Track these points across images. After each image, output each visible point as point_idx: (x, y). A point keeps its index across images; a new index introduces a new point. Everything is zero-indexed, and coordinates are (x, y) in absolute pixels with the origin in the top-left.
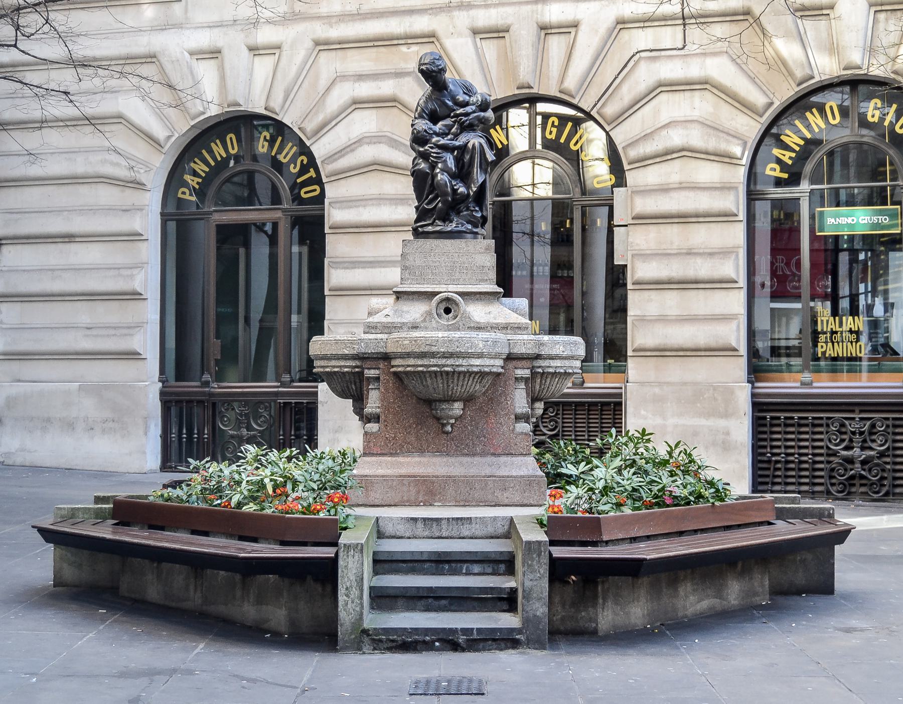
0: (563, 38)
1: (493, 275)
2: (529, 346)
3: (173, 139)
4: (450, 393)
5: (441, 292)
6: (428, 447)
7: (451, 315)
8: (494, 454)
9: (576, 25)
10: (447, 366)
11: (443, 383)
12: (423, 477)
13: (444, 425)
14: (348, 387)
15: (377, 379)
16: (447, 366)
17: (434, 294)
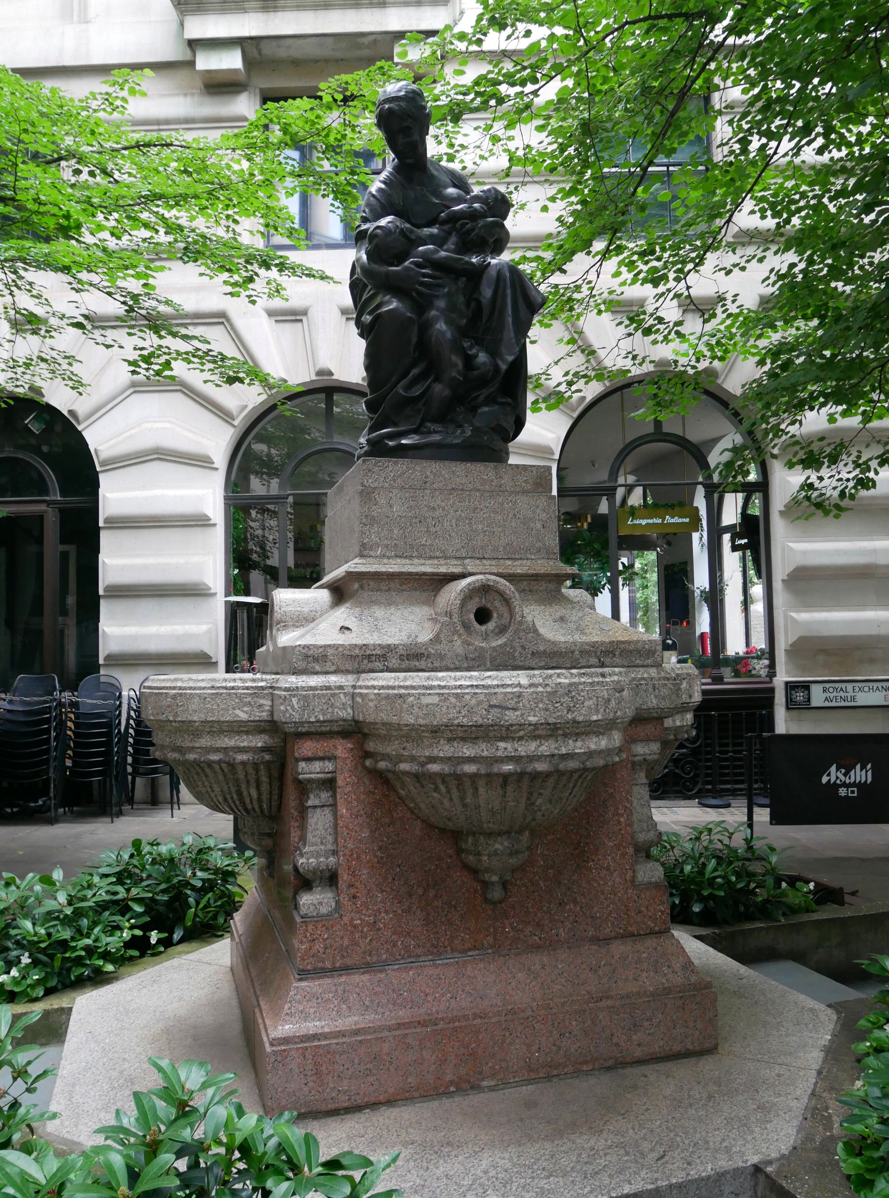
2: (664, 691)
7: (491, 625)
8: (595, 940)
12: (452, 1020)
14: (240, 794)
15: (330, 784)
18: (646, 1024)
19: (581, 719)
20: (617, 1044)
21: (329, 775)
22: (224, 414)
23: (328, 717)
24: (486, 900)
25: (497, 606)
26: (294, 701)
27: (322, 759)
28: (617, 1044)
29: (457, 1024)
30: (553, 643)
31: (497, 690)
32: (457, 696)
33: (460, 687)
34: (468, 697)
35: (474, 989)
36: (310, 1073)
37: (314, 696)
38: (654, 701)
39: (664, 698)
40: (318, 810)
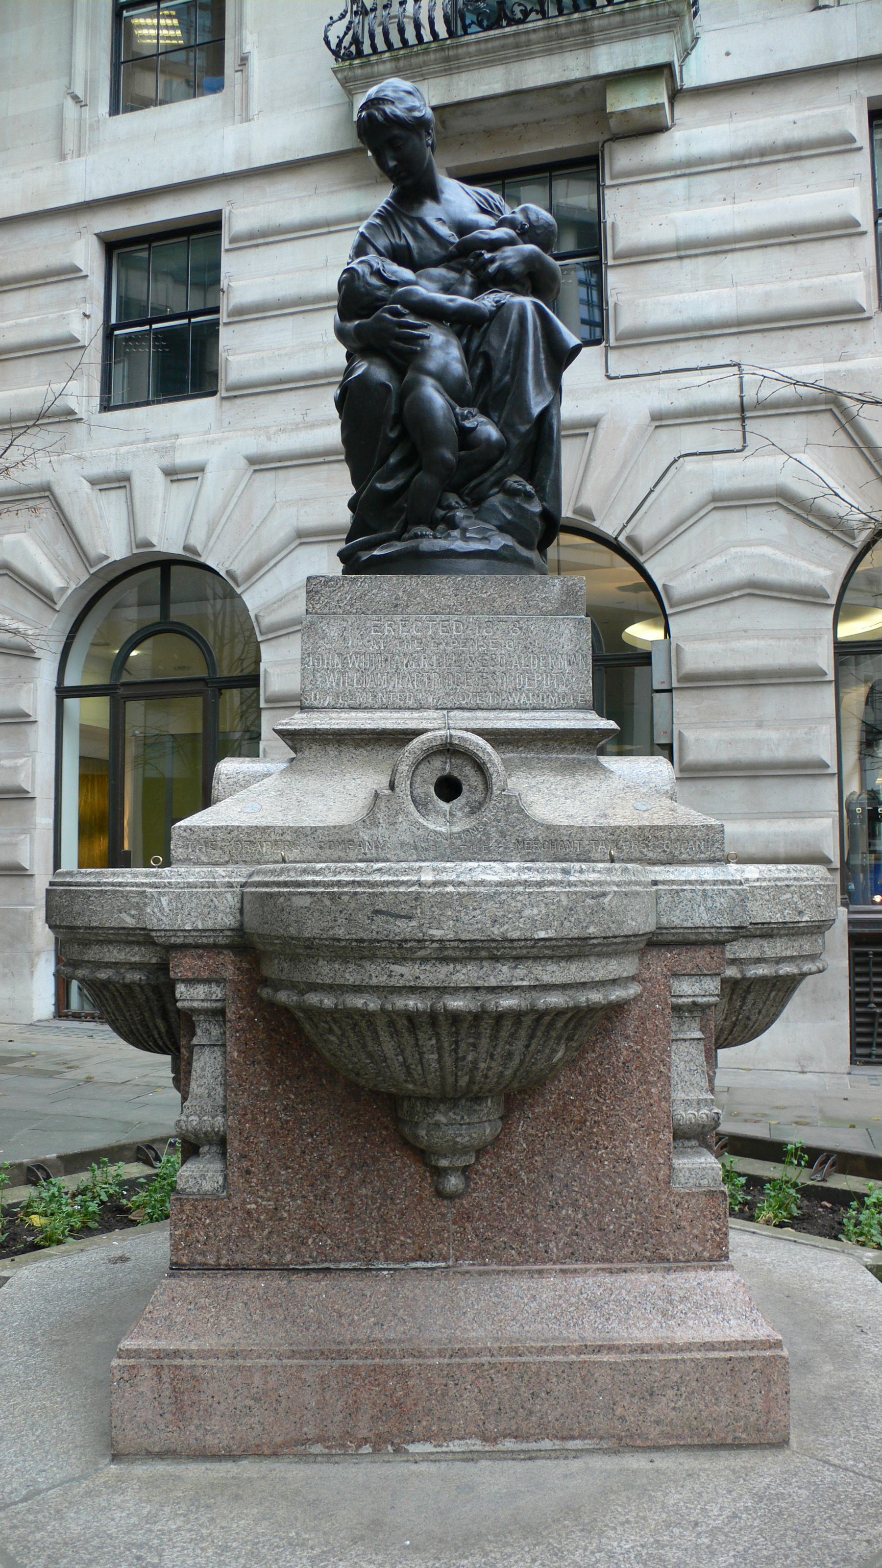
0: (578, 441)
1: (583, 683)
3: (69, 592)
4: (463, 1081)
5: (425, 731)
6: (388, 1241)
9: (594, 424)
10: (456, 990)
11: (440, 1049)
13: (439, 1173)
16: (456, 990)
17: (400, 738)
18: (670, 1393)
19: (516, 935)
20: (622, 1418)
21: (219, 1004)
22: (619, 534)
23: (210, 925)
24: (440, 1194)
25: (469, 778)
26: (164, 901)
27: (207, 981)
28: (622, 1418)
29: (377, 1360)
30: (548, 827)
31: (386, 889)
32: (333, 897)
33: (339, 883)
34: (345, 898)
35: (410, 1315)
36: (167, 1401)
37: (192, 895)
38: (704, 915)
39: (721, 912)
40: (207, 1050)
